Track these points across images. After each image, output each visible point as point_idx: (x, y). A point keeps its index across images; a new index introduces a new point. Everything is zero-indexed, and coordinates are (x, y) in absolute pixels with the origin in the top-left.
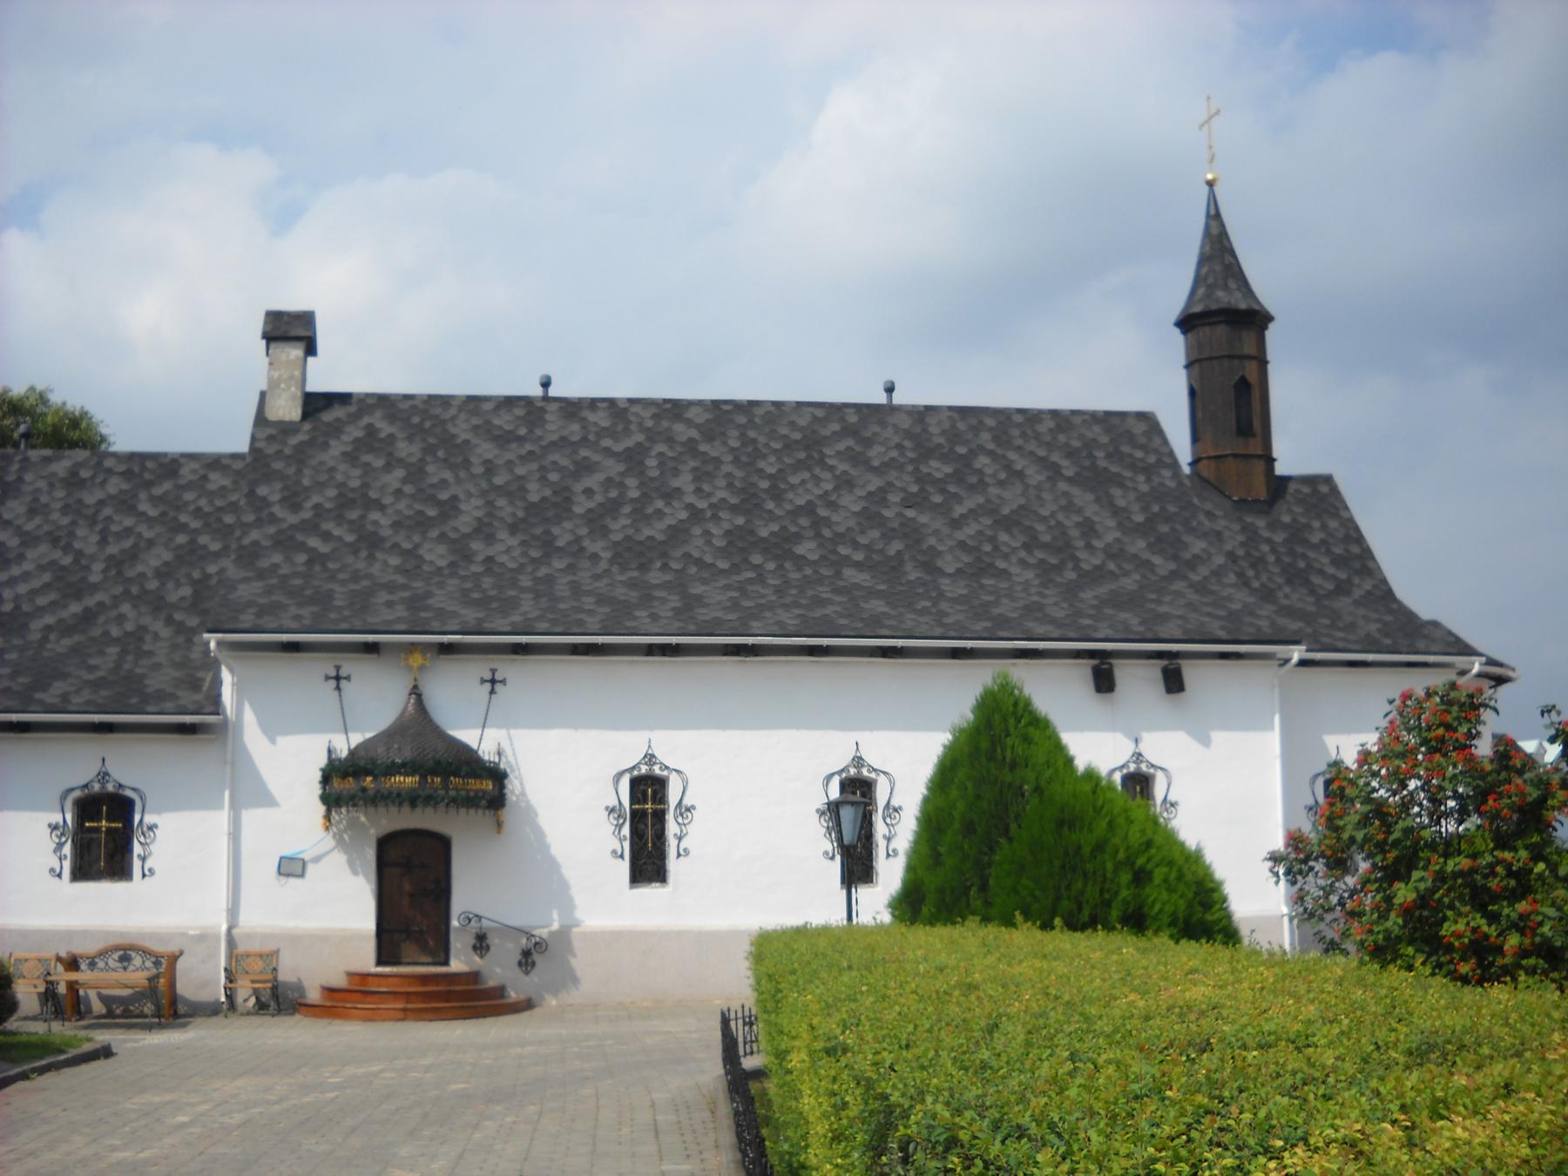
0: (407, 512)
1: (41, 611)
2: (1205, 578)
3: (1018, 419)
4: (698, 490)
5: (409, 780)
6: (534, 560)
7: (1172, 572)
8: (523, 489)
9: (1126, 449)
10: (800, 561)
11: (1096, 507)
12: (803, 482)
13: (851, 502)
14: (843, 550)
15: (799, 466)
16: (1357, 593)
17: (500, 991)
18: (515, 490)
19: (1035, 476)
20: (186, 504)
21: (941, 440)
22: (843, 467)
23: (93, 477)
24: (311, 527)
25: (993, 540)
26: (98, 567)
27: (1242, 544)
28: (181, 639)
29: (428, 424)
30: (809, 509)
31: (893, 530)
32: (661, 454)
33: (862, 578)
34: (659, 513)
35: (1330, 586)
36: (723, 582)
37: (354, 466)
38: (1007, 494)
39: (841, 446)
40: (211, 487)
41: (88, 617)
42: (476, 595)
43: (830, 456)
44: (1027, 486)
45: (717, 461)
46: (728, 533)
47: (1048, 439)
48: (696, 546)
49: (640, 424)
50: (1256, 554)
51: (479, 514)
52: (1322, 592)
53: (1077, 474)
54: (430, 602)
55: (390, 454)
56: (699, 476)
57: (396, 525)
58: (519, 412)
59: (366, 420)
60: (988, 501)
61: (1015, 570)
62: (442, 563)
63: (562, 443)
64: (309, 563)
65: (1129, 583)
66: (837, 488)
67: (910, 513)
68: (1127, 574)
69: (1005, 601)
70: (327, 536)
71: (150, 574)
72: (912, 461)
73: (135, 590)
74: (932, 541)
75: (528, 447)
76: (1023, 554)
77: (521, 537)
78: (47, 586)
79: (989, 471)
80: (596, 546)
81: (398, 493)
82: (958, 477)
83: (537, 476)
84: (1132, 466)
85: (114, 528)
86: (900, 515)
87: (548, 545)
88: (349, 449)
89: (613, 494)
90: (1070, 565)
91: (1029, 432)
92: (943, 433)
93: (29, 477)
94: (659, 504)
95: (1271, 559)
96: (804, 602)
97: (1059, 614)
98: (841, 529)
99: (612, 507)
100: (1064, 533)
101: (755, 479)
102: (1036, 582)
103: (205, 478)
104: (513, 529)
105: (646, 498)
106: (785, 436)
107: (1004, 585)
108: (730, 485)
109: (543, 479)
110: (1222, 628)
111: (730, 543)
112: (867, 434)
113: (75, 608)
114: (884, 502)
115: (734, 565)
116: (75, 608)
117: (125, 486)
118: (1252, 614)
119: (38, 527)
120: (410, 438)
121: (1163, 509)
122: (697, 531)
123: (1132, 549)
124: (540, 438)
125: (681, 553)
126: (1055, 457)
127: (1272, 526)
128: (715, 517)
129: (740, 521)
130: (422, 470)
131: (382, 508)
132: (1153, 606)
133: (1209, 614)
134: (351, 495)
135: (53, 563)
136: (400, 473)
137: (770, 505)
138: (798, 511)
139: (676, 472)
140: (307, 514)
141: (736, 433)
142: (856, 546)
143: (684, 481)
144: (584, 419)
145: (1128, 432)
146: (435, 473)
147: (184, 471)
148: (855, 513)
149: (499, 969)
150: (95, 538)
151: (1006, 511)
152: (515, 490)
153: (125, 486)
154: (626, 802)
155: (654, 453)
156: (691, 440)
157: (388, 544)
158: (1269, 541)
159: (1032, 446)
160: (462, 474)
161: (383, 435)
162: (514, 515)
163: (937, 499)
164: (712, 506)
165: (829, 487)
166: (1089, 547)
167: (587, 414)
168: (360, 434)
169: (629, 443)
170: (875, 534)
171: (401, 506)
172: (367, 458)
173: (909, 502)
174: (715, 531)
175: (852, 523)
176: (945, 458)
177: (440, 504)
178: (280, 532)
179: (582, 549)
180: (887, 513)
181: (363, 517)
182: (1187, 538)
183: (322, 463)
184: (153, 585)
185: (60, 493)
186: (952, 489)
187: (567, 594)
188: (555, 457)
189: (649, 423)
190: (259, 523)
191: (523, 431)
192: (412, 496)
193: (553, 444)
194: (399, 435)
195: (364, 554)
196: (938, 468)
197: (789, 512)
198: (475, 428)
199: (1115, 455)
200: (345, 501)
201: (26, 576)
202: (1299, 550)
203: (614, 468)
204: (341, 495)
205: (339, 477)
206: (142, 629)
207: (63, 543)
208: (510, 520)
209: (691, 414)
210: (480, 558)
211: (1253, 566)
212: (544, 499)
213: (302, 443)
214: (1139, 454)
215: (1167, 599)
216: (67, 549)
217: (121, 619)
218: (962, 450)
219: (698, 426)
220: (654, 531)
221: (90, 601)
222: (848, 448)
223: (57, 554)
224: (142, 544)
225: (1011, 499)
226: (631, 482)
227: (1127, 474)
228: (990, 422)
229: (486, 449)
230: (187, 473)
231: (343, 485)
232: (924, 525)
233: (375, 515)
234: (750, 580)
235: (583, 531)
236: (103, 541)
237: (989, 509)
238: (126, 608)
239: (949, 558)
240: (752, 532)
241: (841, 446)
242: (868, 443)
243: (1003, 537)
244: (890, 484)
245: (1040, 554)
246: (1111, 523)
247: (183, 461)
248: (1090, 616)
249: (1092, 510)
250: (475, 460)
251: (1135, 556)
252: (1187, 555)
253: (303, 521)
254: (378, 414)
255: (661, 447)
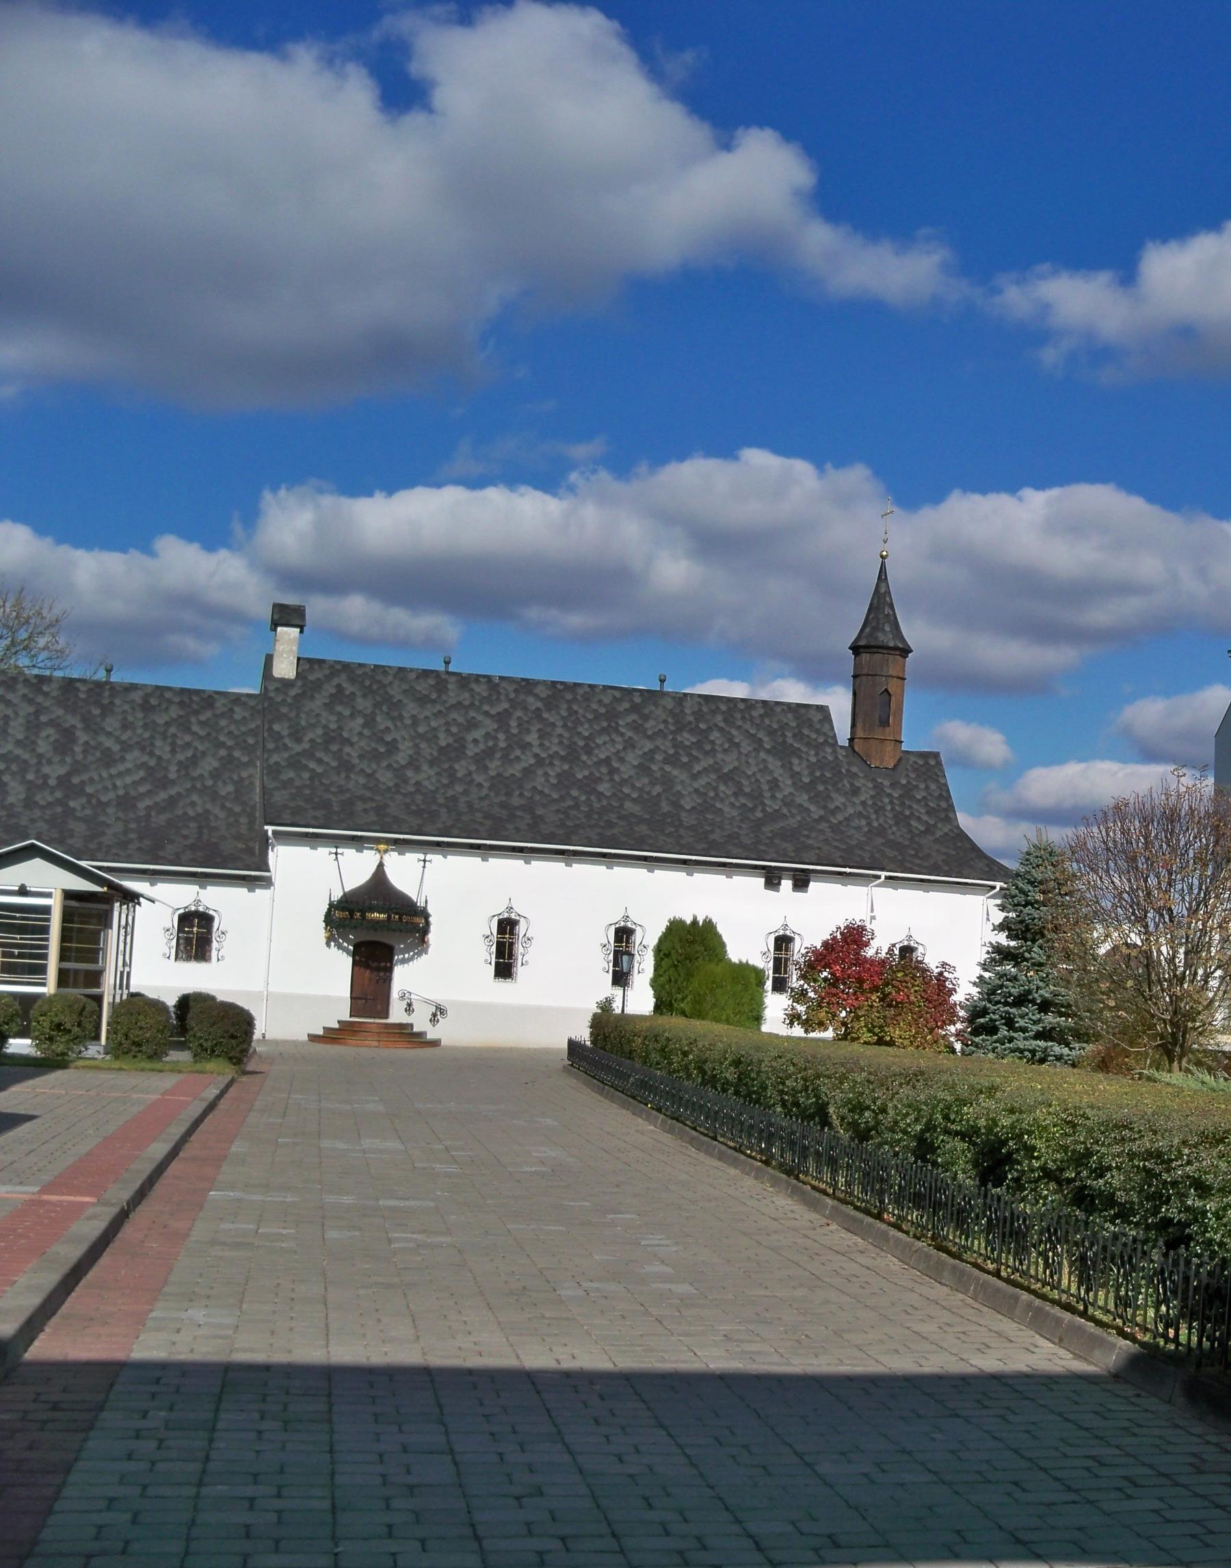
0: (368, 749)
1: (141, 796)
2: (840, 822)
3: (741, 706)
4: (541, 745)
5: (382, 916)
6: (444, 786)
7: (821, 817)
8: (436, 737)
9: (806, 731)
10: (600, 795)
11: (781, 771)
12: (605, 743)
13: (632, 758)
14: (626, 790)
15: (604, 731)
16: (939, 834)
17: (421, 1035)
18: (431, 737)
19: (746, 747)
20: (222, 728)
21: (691, 719)
22: (630, 734)
23: (159, 705)
24: (310, 754)
25: (715, 789)
26: (173, 768)
27: (872, 797)
28: (232, 820)
29: (375, 687)
30: (607, 761)
31: (656, 779)
32: (519, 718)
33: (636, 809)
34: (518, 758)
35: (922, 828)
36: (554, 807)
37: (332, 713)
38: (728, 759)
39: (629, 719)
40: (237, 717)
41: (172, 802)
42: (414, 808)
43: (622, 726)
44: (740, 753)
45: (553, 725)
46: (558, 775)
47: (758, 722)
48: (539, 782)
49: (507, 695)
50: (879, 803)
51: (410, 752)
52: (916, 832)
53: (773, 747)
54: (388, 811)
55: (353, 707)
56: (542, 735)
57: (361, 757)
58: (432, 682)
59: (335, 681)
60: (716, 763)
61: (726, 809)
62: (391, 784)
63: (458, 706)
64: (311, 779)
65: (793, 822)
66: (625, 748)
67: (668, 768)
68: (793, 816)
69: (717, 830)
70: (320, 761)
71: (206, 775)
72: (672, 732)
73: (199, 785)
74: (679, 788)
75: (438, 707)
76: (732, 799)
77: (436, 769)
78: (143, 779)
79: (718, 742)
80: (479, 778)
81: (360, 734)
82: (699, 745)
83: (444, 729)
84: (808, 744)
85: (179, 742)
86: (662, 769)
87: (452, 773)
88: (328, 701)
89: (491, 744)
90: (760, 808)
91: (747, 716)
92: (694, 713)
93: (117, 702)
94: (518, 752)
95: (889, 808)
96: (602, 824)
97: (747, 841)
98: (626, 777)
99: (490, 753)
100: (759, 787)
101: (576, 739)
102: (738, 818)
103: (231, 710)
104: (432, 763)
105: (509, 748)
106: (596, 710)
107: (718, 819)
108: (561, 743)
109: (448, 731)
110: (841, 857)
111: (559, 782)
112: (646, 711)
113: (163, 795)
114: (652, 759)
115: (561, 797)
116: (163, 795)
117: (181, 713)
118: (862, 849)
119: (130, 738)
120: (364, 696)
121: (823, 775)
122: (540, 772)
123: (799, 801)
124: (445, 702)
125: (530, 787)
126: (760, 735)
127: (892, 785)
128: (551, 764)
129: (566, 767)
130: (374, 720)
131: (352, 744)
132: (803, 839)
133: (836, 847)
134: (332, 734)
135: (144, 764)
136: (360, 721)
137: (584, 758)
138: (600, 763)
139: (528, 731)
140: (306, 746)
141: (565, 706)
142: (633, 787)
143: (532, 738)
144: (472, 690)
145: (810, 719)
146: (382, 722)
147: (218, 705)
148: (635, 767)
149: (420, 1022)
150: (168, 748)
151: (726, 771)
152: (431, 737)
153: (181, 713)
154: (495, 932)
155: (515, 717)
156: (538, 709)
157: (357, 769)
158: (889, 795)
159: (747, 726)
160: (399, 724)
161: (347, 693)
162: (431, 754)
163: (685, 759)
164: (550, 756)
165: (620, 747)
166: (773, 797)
167: (474, 686)
168: (333, 691)
169: (500, 709)
170: (646, 780)
171: (363, 744)
172: (339, 708)
173: (666, 761)
174: (551, 773)
175: (632, 773)
176: (691, 731)
177: (387, 743)
178: (291, 757)
179: (472, 781)
180: (654, 768)
181: (340, 750)
182: (833, 795)
183: (312, 710)
184: (209, 783)
185: (140, 715)
186: (694, 753)
187: (466, 810)
188: (454, 715)
189: (512, 696)
190: (277, 750)
191: (434, 696)
192: (369, 737)
193: (453, 706)
194: (358, 694)
195: (343, 775)
196: (687, 738)
197: (596, 763)
198: (405, 691)
199: (798, 736)
200: (329, 739)
201: (128, 771)
202: (907, 803)
203: (490, 725)
204: (325, 734)
205: (324, 722)
206: (207, 811)
207: (148, 750)
208: (428, 757)
209: (539, 690)
210: (413, 781)
211: (876, 812)
212: (448, 745)
213: (297, 695)
214: (814, 736)
215: (814, 835)
216: (151, 754)
217: (193, 804)
218: (703, 726)
219: (541, 699)
220: (515, 770)
221: (173, 791)
222: (634, 721)
223: (145, 758)
224: (199, 754)
225: (730, 762)
226: (501, 736)
227: (804, 749)
228: (723, 707)
229: (411, 708)
230: (220, 704)
231: (325, 727)
232: (675, 777)
233: (347, 749)
234: (569, 807)
235: (473, 768)
236: (173, 751)
237: (716, 768)
238: (195, 797)
239: (688, 799)
240: (574, 775)
241: (629, 719)
242: (646, 718)
243: (722, 788)
244: (657, 748)
245: (743, 800)
246: (789, 782)
247: (216, 696)
248: (766, 845)
249: (778, 772)
250: (405, 714)
251: (801, 805)
252: (832, 806)
253: (304, 750)
254: (344, 676)
255: (519, 713)
